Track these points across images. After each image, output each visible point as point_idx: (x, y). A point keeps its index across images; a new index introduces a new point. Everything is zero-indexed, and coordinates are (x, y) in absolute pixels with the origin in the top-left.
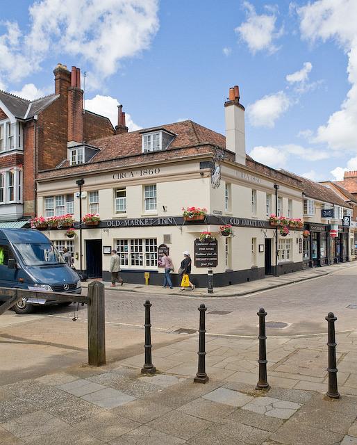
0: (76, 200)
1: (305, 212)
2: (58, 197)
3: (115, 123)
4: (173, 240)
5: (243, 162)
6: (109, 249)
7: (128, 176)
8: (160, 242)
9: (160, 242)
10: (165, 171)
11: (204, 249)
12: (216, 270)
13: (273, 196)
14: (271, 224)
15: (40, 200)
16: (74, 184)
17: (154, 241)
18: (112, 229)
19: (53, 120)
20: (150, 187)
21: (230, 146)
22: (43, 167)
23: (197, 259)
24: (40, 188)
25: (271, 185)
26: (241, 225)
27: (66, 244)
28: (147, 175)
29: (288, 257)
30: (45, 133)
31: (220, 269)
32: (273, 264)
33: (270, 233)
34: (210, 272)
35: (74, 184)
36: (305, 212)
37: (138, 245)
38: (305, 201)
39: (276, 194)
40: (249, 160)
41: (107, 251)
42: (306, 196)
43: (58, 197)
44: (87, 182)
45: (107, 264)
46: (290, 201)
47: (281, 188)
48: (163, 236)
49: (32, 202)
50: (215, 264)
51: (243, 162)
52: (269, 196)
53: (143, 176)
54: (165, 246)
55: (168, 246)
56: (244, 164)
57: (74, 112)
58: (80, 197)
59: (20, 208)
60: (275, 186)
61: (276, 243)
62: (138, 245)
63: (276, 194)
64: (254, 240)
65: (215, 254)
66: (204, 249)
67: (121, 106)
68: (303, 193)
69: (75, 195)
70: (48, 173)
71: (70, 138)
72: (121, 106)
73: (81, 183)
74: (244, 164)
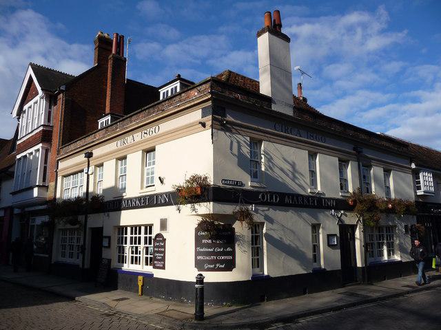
3: (81, 266)
4: (170, 225)
5: (289, 112)
6: (107, 245)
9: (156, 230)
16: (81, 158)
17: (149, 228)
23: (199, 258)
34: (200, 279)
35: (81, 158)
37: (138, 236)
40: (301, 106)
41: (105, 243)
44: (97, 152)
52: (343, 163)
55: (165, 235)
58: (87, 173)
62: (138, 236)
69: (85, 172)
73: (89, 155)
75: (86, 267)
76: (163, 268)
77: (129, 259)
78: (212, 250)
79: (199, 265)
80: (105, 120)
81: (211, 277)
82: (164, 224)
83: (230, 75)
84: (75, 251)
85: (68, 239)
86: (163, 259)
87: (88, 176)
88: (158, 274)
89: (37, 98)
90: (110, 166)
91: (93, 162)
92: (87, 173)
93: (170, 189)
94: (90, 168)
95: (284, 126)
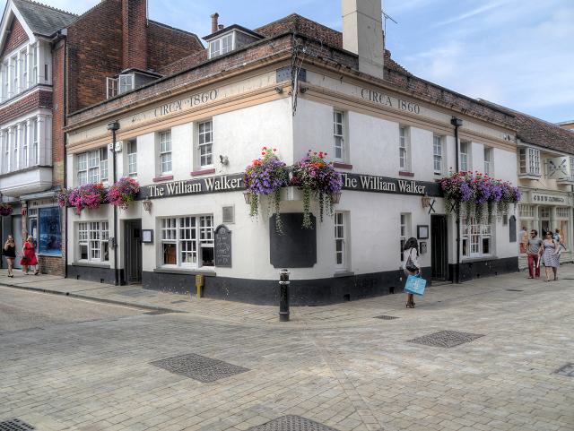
0: (110, 154)
1: (523, 170)
2: (89, 152)
5: (379, 73)
7: (173, 109)
8: (218, 221)
9: (218, 221)
10: (225, 93)
13: (450, 140)
14: (438, 189)
15: (70, 159)
17: (208, 219)
18: (157, 200)
19: (96, 36)
20: (203, 126)
21: (350, 44)
22: (76, 106)
24: (72, 140)
25: (445, 119)
26: (360, 188)
27: (178, 224)
28: (199, 104)
29: (486, 250)
30: (82, 56)
31: (325, 267)
32: (452, 260)
33: (439, 206)
34: (285, 277)
35: (104, 130)
36: (523, 170)
37: (190, 228)
38: (521, 152)
39: (456, 136)
40: (392, 69)
42: (522, 141)
43: (89, 152)
44: (125, 123)
45: (150, 259)
46: (487, 151)
47: (467, 125)
48: (221, 209)
49: (62, 163)
51: (379, 73)
52: (439, 139)
53: (194, 106)
54: (224, 227)
55: (230, 227)
56: (382, 78)
57: (131, 23)
58: (113, 150)
59: (48, 173)
60: (454, 121)
61: (458, 222)
62: (190, 228)
63: (456, 136)
64: (404, 217)
67: (217, 15)
68: (518, 137)
69: (109, 148)
70: (78, 116)
71: (126, 62)
72: (217, 15)
73: (115, 128)
74: (382, 78)
75: (119, 268)
76: (228, 264)
77: (106, 263)
79: (276, 261)
80: (128, 81)
81: (296, 274)
82: (228, 213)
83: (297, 20)
84: (100, 249)
85: (88, 234)
86: (230, 259)
87: (115, 153)
88: (221, 272)
89: (27, 45)
90: (147, 144)
91: (121, 137)
92: (113, 150)
93: (242, 170)
94: (117, 144)
95: (372, 93)
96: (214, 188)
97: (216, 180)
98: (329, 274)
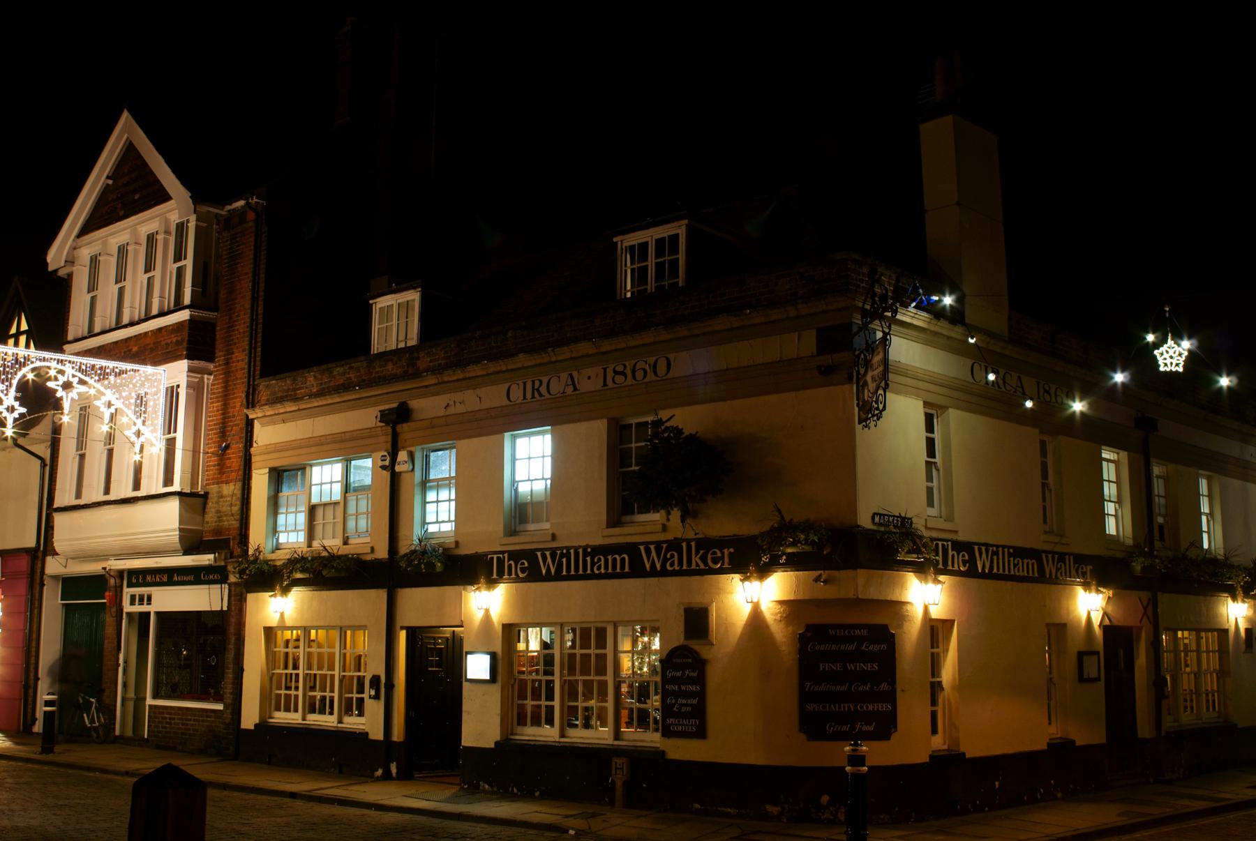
11: (838, 667)
12: (877, 753)
23: (810, 707)
32: (1144, 730)
50: (885, 727)
65: (884, 687)
66: (838, 667)
76: (701, 733)
77: (353, 722)
78: (844, 688)
96: (663, 566)
97: (562, 555)
98: (920, 756)
